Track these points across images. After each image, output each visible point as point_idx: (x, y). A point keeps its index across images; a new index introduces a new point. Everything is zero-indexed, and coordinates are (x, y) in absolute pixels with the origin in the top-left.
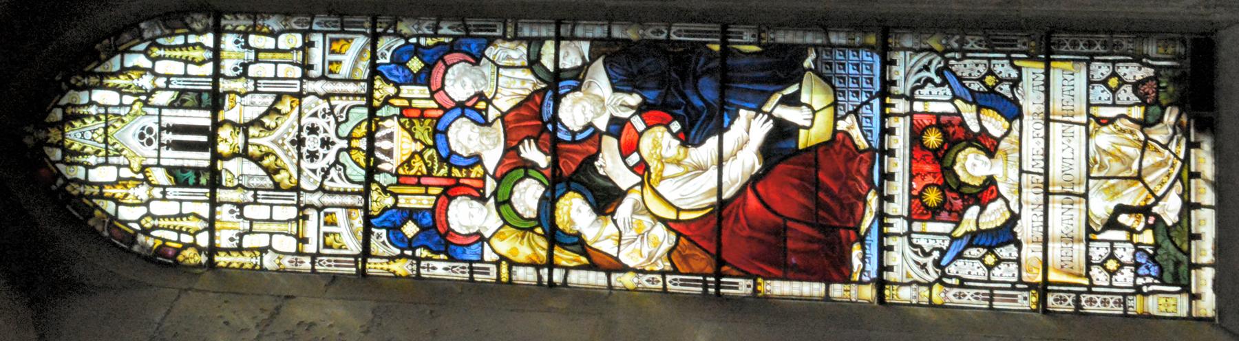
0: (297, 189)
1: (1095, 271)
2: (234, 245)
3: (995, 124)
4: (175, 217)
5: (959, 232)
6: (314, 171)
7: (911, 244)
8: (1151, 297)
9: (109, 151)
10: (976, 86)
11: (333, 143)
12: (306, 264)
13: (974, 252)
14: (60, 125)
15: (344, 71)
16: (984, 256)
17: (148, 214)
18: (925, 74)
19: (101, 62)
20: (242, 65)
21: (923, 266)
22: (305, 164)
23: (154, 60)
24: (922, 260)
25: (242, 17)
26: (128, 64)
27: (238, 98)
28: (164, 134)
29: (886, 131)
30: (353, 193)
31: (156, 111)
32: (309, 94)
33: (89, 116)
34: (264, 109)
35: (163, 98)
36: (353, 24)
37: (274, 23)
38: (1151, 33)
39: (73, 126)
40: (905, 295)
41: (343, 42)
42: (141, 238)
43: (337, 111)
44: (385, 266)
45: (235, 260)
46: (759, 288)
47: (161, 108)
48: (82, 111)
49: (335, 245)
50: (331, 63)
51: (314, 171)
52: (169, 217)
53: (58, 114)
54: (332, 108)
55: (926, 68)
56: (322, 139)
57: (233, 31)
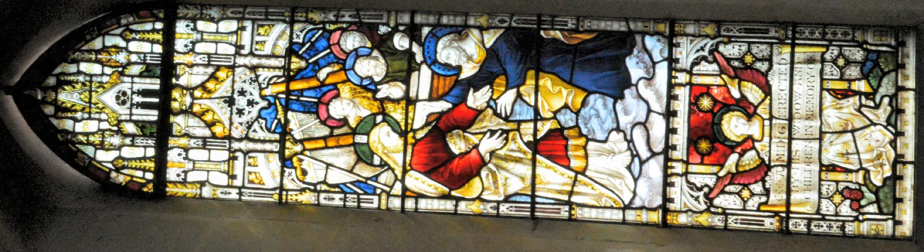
0: (229, 138)
1: (825, 203)
2: (180, 179)
3: (753, 93)
4: (140, 159)
5: (722, 174)
6: (241, 124)
7: (688, 182)
8: (865, 223)
9: (90, 109)
10: (736, 64)
11: (257, 103)
12: (234, 195)
13: (731, 188)
14: (56, 89)
15: (267, 50)
16: (741, 191)
17: (120, 157)
18: (701, 53)
19: (87, 42)
20: (191, 42)
21: (697, 199)
22: (236, 118)
23: (128, 41)
24: (695, 194)
25: (191, 7)
26: (108, 44)
27: (187, 69)
28: (134, 96)
29: (671, 97)
30: (271, 141)
31: (129, 79)
32: (240, 66)
33: (77, 82)
34: (206, 77)
35: (136, 70)
36: (273, 14)
37: (214, 13)
38: (869, 26)
39: (64, 90)
40: (683, 219)
41: (266, 27)
42: (113, 174)
43: (261, 79)
44: (294, 198)
45: (180, 190)
46: (573, 212)
47: (132, 77)
48: (72, 78)
49: (256, 181)
50: (257, 43)
51: (241, 124)
52: (135, 159)
53: (52, 81)
54: (257, 77)
55: (702, 49)
56: (248, 100)
57: (185, 18)
